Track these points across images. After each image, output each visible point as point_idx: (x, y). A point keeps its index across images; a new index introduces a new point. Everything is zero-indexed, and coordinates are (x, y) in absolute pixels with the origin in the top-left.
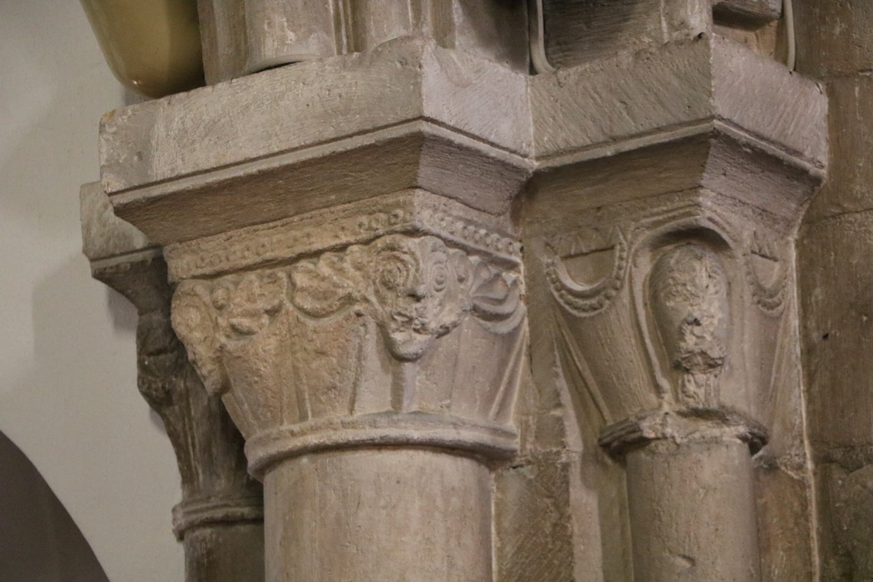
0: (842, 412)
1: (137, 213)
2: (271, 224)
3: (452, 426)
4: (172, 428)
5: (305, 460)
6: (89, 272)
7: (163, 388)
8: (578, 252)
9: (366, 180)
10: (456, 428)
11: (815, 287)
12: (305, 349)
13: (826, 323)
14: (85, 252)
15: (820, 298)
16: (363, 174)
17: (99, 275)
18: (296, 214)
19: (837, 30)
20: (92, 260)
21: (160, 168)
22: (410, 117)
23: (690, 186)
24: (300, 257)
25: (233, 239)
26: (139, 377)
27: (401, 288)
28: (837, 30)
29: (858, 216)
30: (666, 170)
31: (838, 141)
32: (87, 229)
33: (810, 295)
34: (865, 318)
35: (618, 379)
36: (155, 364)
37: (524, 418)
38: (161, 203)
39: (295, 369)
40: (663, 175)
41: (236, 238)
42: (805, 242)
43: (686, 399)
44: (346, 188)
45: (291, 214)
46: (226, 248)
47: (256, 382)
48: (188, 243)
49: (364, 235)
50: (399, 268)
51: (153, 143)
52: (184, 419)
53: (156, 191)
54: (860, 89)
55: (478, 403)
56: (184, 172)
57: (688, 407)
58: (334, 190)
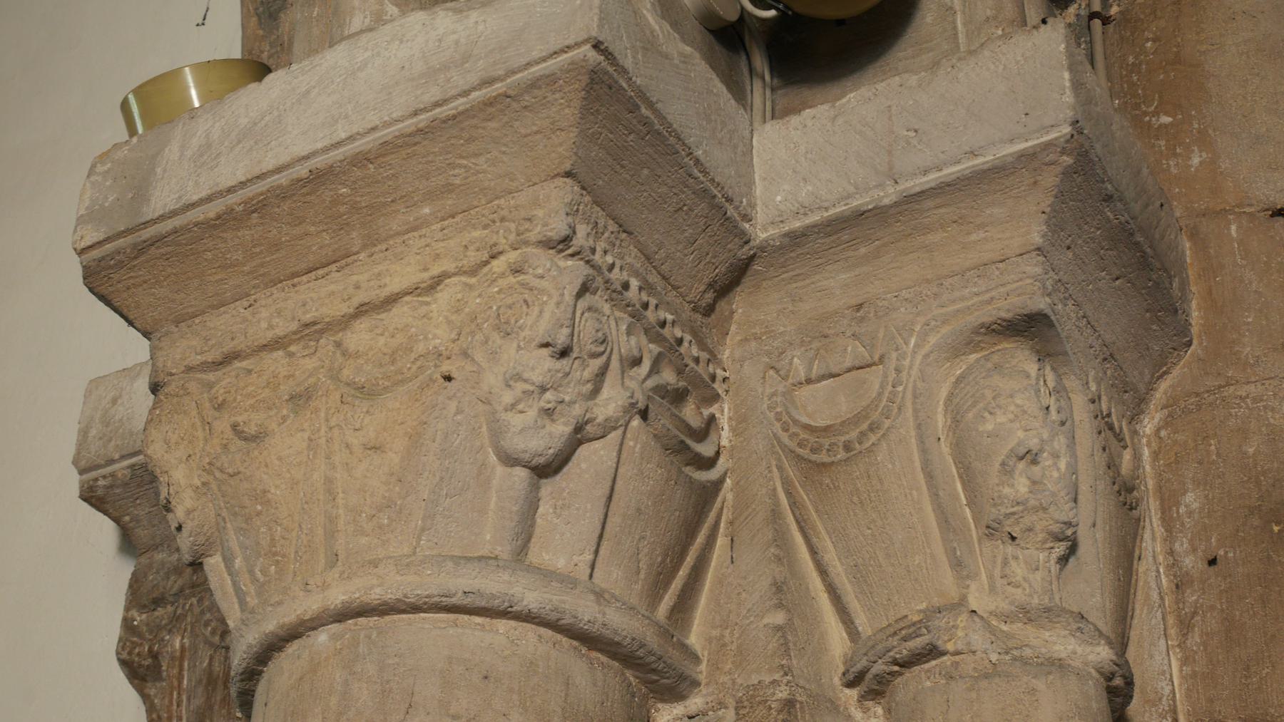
0: (1248, 668)
1: (116, 277)
2: (321, 272)
3: (592, 597)
4: (154, 716)
5: (322, 637)
6: (76, 491)
7: (150, 650)
8: (822, 372)
9: (484, 172)
10: (598, 603)
11: (1184, 494)
12: (347, 446)
13: (1208, 540)
14: (75, 463)
15: (1195, 505)
16: (482, 160)
17: (92, 497)
18: (364, 247)
19: (1196, 160)
20: (81, 472)
21: (162, 199)
22: (570, 42)
23: (1018, 252)
24: (362, 310)
25: (257, 305)
26: (120, 640)
27: (526, 333)
28: (1196, 160)
29: (1252, 388)
30: (982, 226)
31: (1210, 293)
32: (84, 433)
33: (1178, 504)
34: (1276, 529)
35: (888, 556)
36: (147, 625)
37: (715, 633)
38: (153, 250)
39: (329, 481)
40: (974, 237)
41: (263, 302)
42: (1163, 433)
43: (1009, 589)
44: (449, 188)
45: (355, 249)
46: (245, 320)
47: (259, 514)
48: (190, 322)
49: (473, 257)
50: (525, 301)
51: (159, 170)
52: (171, 694)
53: (147, 234)
54: (1239, 228)
55: (642, 576)
56: (195, 198)
57: (1011, 603)
58: (430, 196)
